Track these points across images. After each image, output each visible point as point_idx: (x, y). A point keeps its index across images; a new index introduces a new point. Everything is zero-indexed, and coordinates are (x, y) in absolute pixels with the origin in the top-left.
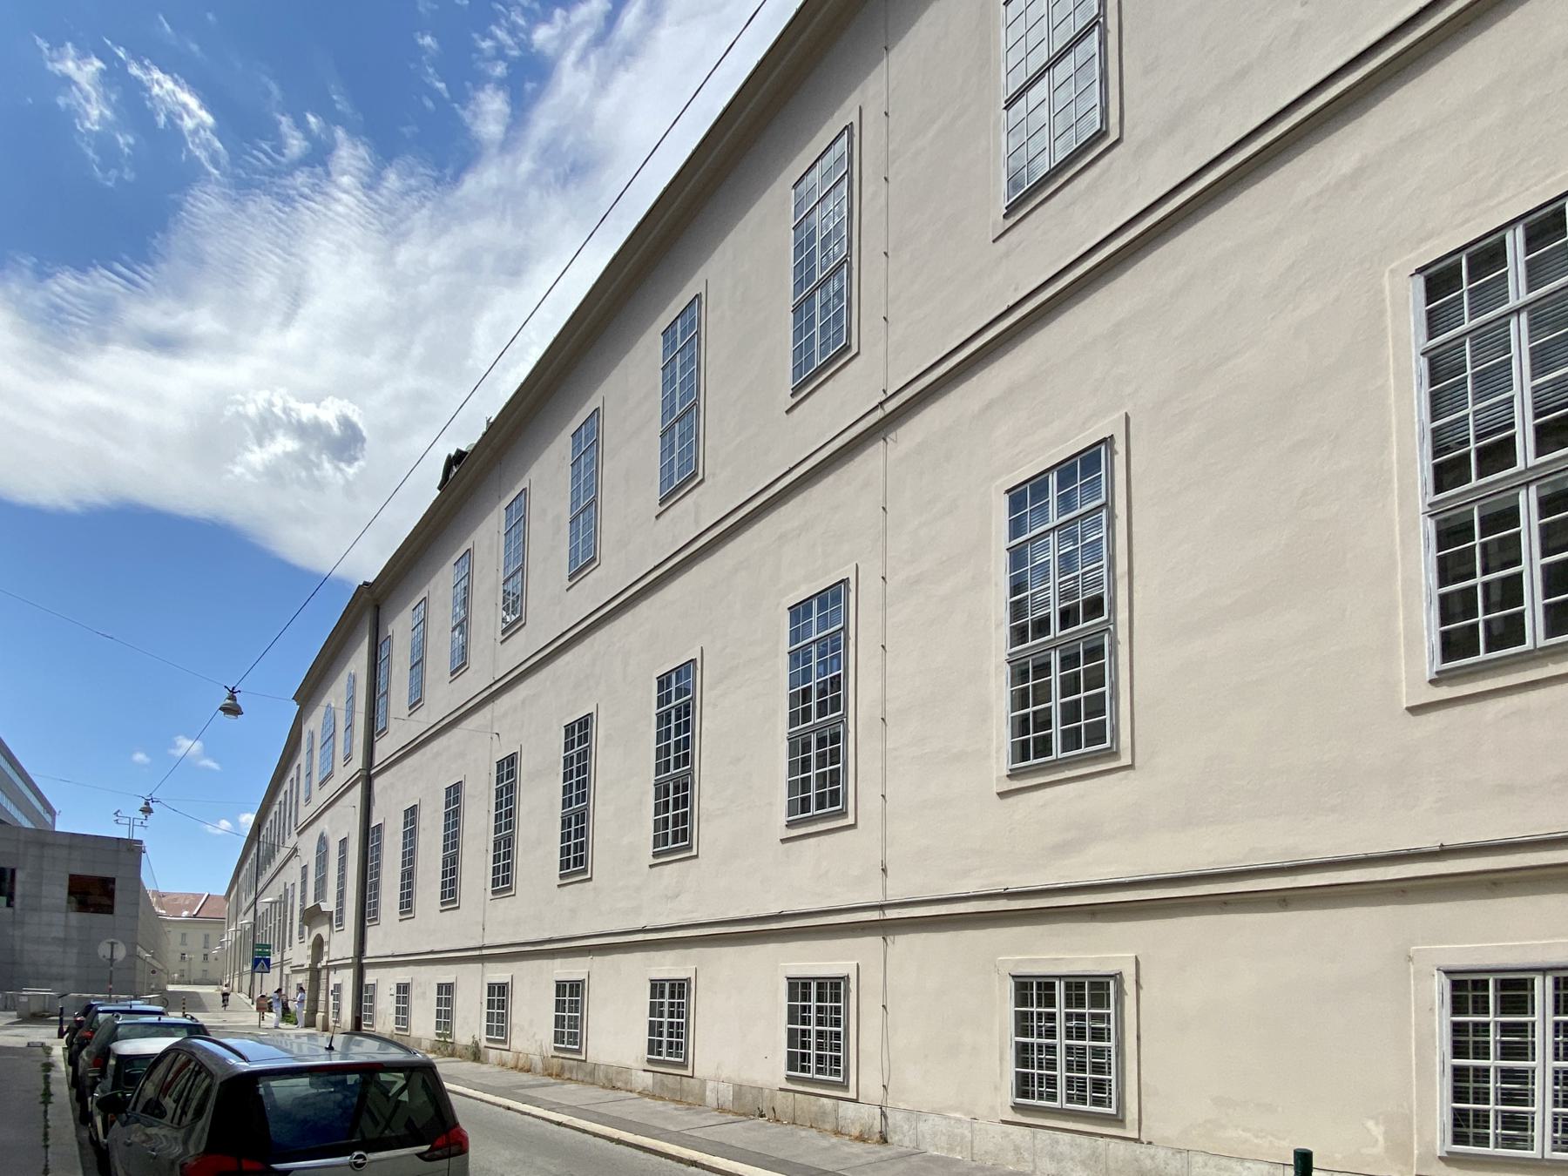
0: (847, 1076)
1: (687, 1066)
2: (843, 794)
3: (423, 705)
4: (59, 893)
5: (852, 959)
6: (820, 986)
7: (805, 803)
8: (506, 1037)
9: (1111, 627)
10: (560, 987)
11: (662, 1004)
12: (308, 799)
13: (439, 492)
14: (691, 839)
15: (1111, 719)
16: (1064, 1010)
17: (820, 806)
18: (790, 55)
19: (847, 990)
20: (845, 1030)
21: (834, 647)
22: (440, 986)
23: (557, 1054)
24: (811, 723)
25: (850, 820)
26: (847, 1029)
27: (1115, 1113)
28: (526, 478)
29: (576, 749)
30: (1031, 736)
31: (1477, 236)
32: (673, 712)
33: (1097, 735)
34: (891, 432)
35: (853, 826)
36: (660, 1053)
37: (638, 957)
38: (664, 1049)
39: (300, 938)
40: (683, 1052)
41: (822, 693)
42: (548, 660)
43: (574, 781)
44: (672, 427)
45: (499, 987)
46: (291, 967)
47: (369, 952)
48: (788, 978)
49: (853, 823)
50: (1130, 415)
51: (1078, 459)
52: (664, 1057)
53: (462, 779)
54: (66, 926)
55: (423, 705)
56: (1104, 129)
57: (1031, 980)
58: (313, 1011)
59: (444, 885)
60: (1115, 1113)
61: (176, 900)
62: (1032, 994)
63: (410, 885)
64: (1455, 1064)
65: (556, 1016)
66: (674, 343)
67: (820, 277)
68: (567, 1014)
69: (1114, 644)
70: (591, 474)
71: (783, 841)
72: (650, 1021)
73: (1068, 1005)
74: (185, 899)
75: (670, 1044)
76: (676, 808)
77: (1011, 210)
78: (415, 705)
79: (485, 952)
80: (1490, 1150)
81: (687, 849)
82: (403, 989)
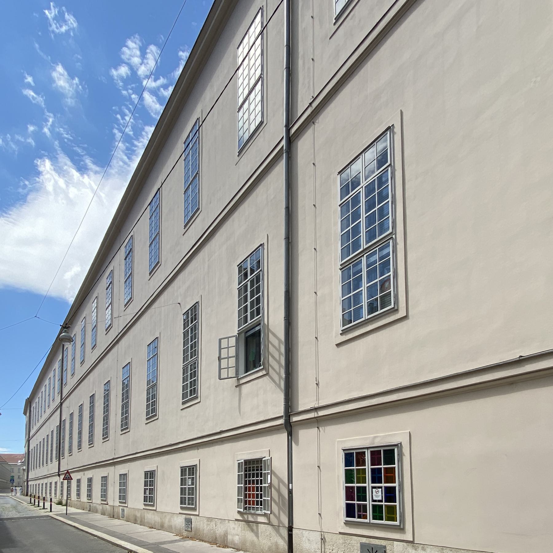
1: (196, 509)
2: (197, 389)
3: (133, 300)
5: (198, 458)
8: (196, 506)
9: (394, 236)
10: (183, 470)
15: (394, 291)
16: (370, 467)
19: (401, 455)
20: (399, 485)
22: (146, 473)
24: (248, 323)
27: (399, 524)
31: (357, 155)
34: (316, 120)
37: (227, 447)
41: (252, 307)
45: (150, 473)
48: (344, 450)
49: (405, 315)
50: (402, 110)
55: (133, 300)
56: (262, 121)
57: (352, 451)
60: (399, 524)
61: (16, 456)
63: (127, 412)
64: (372, 486)
65: (181, 488)
71: (78, 452)
74: (20, 456)
79: (321, 413)
80: (367, 521)
81: (155, 416)
82: (150, 476)
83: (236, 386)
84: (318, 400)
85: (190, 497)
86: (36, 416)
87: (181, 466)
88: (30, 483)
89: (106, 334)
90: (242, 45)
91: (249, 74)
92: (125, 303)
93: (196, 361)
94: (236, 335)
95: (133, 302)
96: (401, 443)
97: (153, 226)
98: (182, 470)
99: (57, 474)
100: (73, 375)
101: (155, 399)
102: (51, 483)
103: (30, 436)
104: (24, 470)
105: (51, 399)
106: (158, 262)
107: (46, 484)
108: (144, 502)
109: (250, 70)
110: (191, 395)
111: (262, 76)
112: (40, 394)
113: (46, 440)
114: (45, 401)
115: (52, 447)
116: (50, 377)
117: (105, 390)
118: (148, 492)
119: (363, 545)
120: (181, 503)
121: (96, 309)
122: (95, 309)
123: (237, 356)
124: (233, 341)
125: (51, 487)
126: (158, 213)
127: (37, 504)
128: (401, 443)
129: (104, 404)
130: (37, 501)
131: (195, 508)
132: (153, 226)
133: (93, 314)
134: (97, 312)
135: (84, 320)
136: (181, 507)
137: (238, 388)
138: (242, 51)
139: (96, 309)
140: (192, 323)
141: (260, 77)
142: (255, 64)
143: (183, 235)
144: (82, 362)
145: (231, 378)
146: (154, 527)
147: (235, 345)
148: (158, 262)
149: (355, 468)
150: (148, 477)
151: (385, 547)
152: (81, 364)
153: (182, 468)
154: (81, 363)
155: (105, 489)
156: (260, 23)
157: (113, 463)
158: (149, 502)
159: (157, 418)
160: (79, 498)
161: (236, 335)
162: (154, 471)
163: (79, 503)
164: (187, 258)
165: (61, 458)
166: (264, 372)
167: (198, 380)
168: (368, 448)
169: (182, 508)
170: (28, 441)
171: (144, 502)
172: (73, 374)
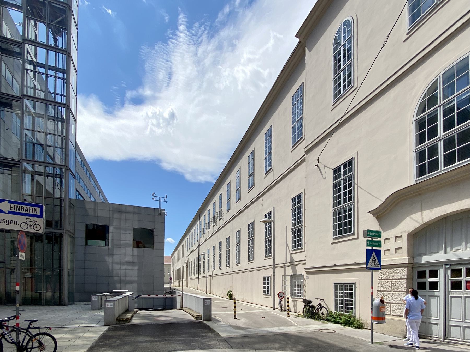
4: (128, 238)
6: (345, 286)
7: (340, 233)
9: (353, 203)
13: (297, 40)
14: (303, 246)
16: (344, 291)
17: (298, 247)
19: (355, 287)
20: (355, 299)
21: (349, 183)
25: (303, 250)
26: (355, 299)
29: (297, 206)
30: (348, 227)
32: (296, 208)
33: (350, 230)
35: (304, 251)
43: (267, 230)
44: (295, 124)
46: (306, 269)
51: (455, 98)
53: (302, 191)
54: (133, 255)
58: (281, 307)
59: (249, 255)
66: (296, 99)
67: (343, 68)
69: (354, 207)
70: (270, 145)
72: (335, 299)
73: (345, 290)
76: (298, 237)
78: (228, 210)
89: (291, 152)
96: (355, 283)
114: (195, 238)
128: (355, 283)
143: (331, 111)
149: (338, 291)
152: (249, 190)
168: (343, 284)
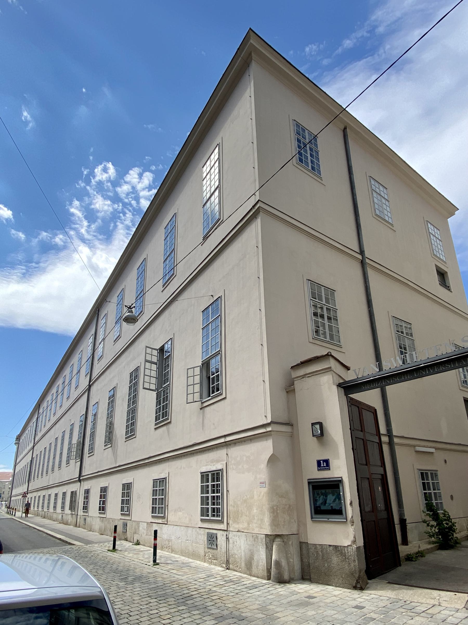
0: (223, 517)
3: (121, 337)
9: (220, 352)
11: (208, 486)
12: (44, 426)
18: (130, 249)
22: (124, 485)
23: (154, 521)
26: (222, 494)
27: (221, 519)
28: (124, 284)
36: (208, 516)
38: (210, 513)
39: (41, 476)
40: (221, 514)
42: (133, 343)
45: (127, 485)
47: (83, 474)
49: (225, 397)
52: (210, 518)
55: (121, 337)
60: (221, 519)
62: (219, 477)
68: (426, 481)
71: (66, 467)
75: (213, 510)
77: (86, 376)
79: (229, 439)
82: (127, 487)
83: (201, 409)
84: (116, 462)
85: (204, 507)
86: (29, 438)
87: (201, 472)
88: (12, 499)
90: (206, 166)
91: (210, 184)
92: (115, 339)
93: (169, 387)
94: (200, 366)
95: (120, 339)
97: (139, 284)
98: (202, 476)
99: (78, 479)
100: (76, 388)
101: (134, 420)
102: (39, 497)
103: (35, 442)
104: (9, 488)
105: (47, 419)
106: (142, 311)
107: (39, 497)
108: (121, 511)
109: (211, 181)
110: (163, 418)
111: (219, 186)
112: (25, 434)
113: (48, 449)
115: (26, 473)
116: (48, 400)
117: (80, 421)
118: (102, 502)
119: (208, 534)
120: (202, 515)
121: (104, 324)
122: (91, 344)
123: (201, 383)
124: (198, 371)
125: (43, 500)
126: (143, 276)
127: (14, 514)
129: (79, 432)
130: (14, 512)
131: (221, 520)
132: (139, 284)
133: (89, 348)
134: (105, 327)
135: (81, 353)
136: (152, 516)
137: (202, 410)
138: (206, 169)
139: (104, 324)
140: (135, 380)
141: (218, 187)
142: (206, 189)
144: (68, 398)
145: (196, 401)
146: (56, 520)
147: (199, 374)
148: (142, 311)
150: (125, 489)
151: (217, 534)
153: (202, 474)
154: (67, 399)
155: (162, 498)
156: (218, 153)
157: (47, 488)
158: (102, 511)
159: (135, 436)
160: (63, 511)
161: (200, 366)
162: (220, 470)
163: (34, 511)
164: (196, 272)
165: (30, 482)
166: (110, 446)
167: (135, 422)
169: (202, 520)
170: (15, 466)
171: (121, 511)
172: (61, 406)
